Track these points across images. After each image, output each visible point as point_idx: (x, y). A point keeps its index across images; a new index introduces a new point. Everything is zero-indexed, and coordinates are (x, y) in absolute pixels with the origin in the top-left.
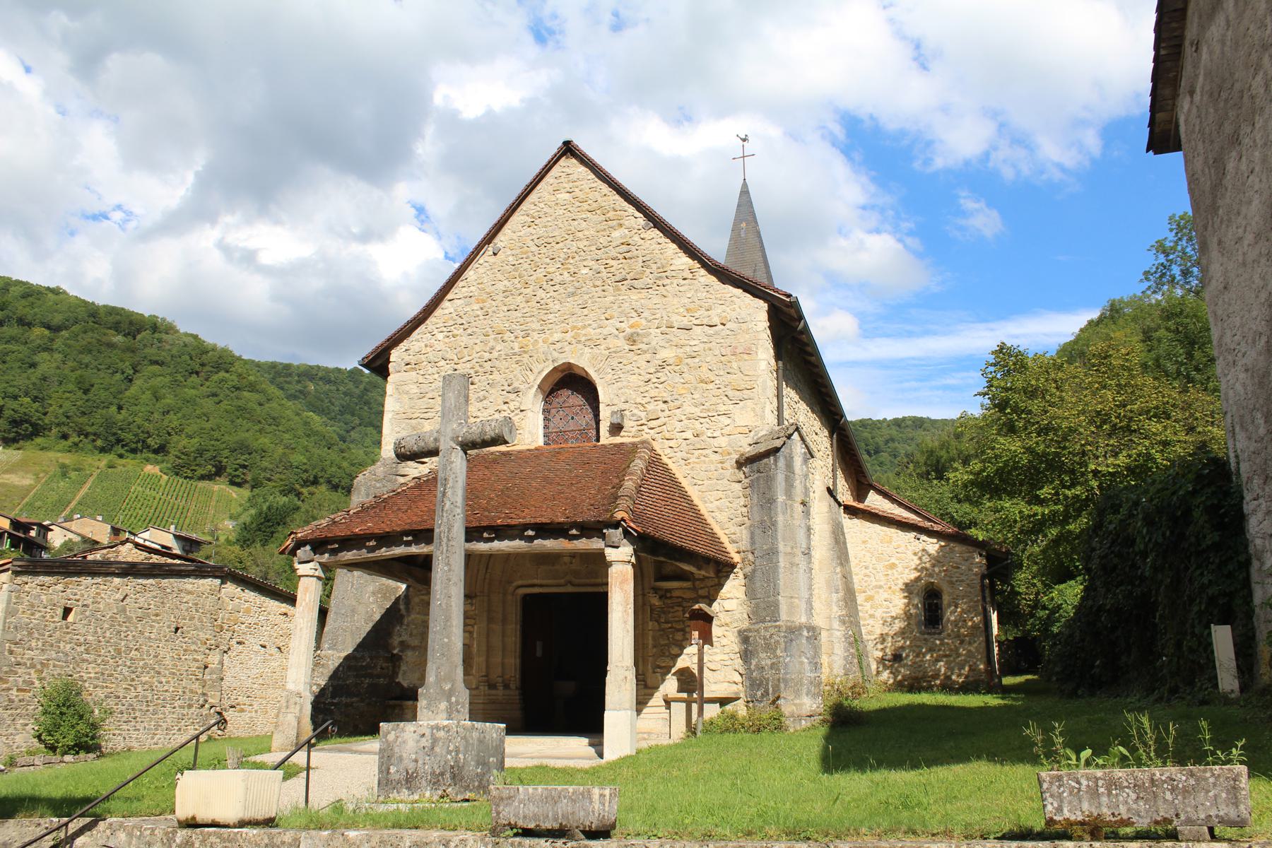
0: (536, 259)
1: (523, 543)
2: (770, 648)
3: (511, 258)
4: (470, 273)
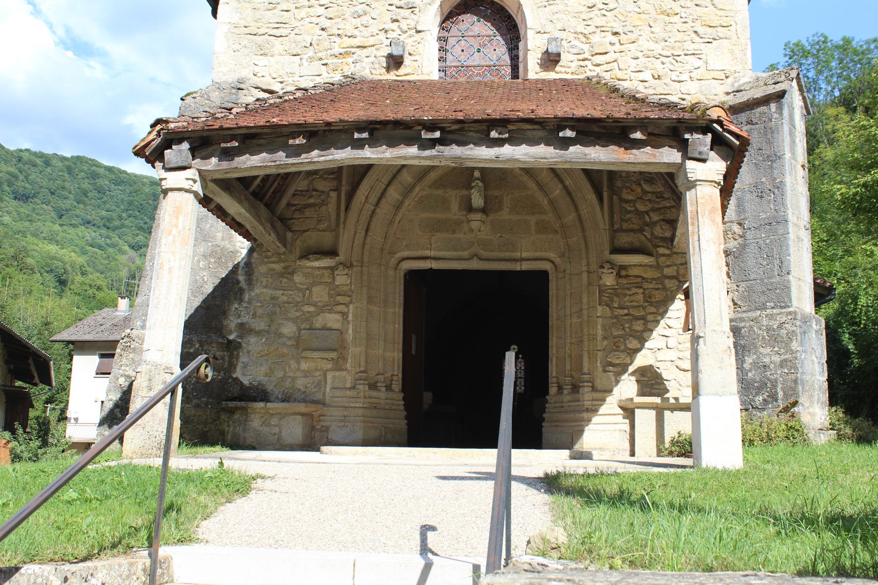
2: (774, 338)
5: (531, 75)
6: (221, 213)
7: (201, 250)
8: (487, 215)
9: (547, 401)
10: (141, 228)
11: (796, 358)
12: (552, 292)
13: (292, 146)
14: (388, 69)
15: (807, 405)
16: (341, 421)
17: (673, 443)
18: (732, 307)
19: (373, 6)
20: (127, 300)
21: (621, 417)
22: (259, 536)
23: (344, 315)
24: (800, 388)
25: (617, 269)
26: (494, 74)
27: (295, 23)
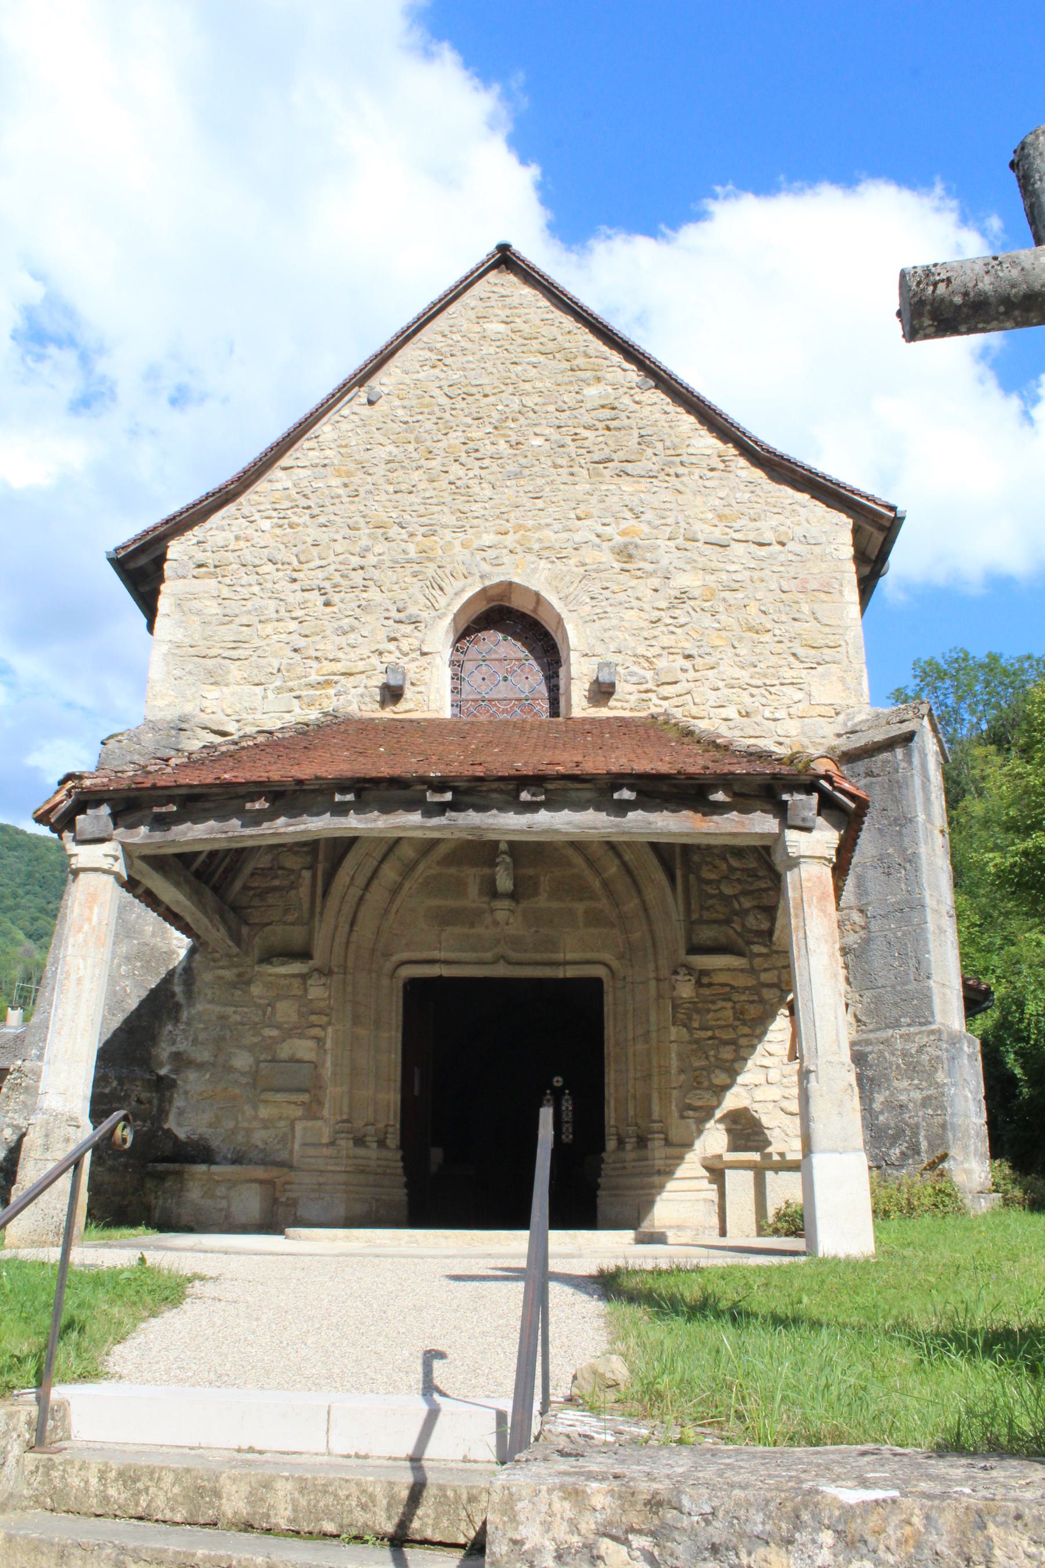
0: (447, 416)
1: (603, 816)
2: (913, 1068)
3: (400, 412)
4: (324, 429)
5: (577, 712)
6: (151, 900)
7: (123, 949)
8: (517, 902)
9: (602, 1161)
10: (42, 910)
11: (943, 1094)
12: (608, 1008)
13: (249, 811)
14: (383, 704)
15: (960, 1158)
16: (314, 1191)
17: (780, 1216)
18: (855, 1024)
19: (363, 620)
20: (19, 1011)
21: (706, 1181)
22: (195, 1368)
23: (320, 1041)
24: (950, 1135)
25: (696, 975)
26: (527, 709)
27: (257, 642)
